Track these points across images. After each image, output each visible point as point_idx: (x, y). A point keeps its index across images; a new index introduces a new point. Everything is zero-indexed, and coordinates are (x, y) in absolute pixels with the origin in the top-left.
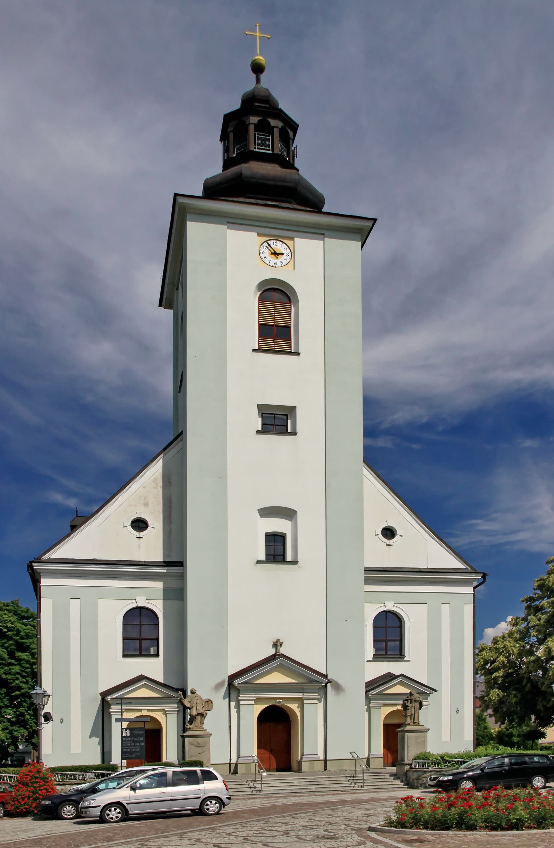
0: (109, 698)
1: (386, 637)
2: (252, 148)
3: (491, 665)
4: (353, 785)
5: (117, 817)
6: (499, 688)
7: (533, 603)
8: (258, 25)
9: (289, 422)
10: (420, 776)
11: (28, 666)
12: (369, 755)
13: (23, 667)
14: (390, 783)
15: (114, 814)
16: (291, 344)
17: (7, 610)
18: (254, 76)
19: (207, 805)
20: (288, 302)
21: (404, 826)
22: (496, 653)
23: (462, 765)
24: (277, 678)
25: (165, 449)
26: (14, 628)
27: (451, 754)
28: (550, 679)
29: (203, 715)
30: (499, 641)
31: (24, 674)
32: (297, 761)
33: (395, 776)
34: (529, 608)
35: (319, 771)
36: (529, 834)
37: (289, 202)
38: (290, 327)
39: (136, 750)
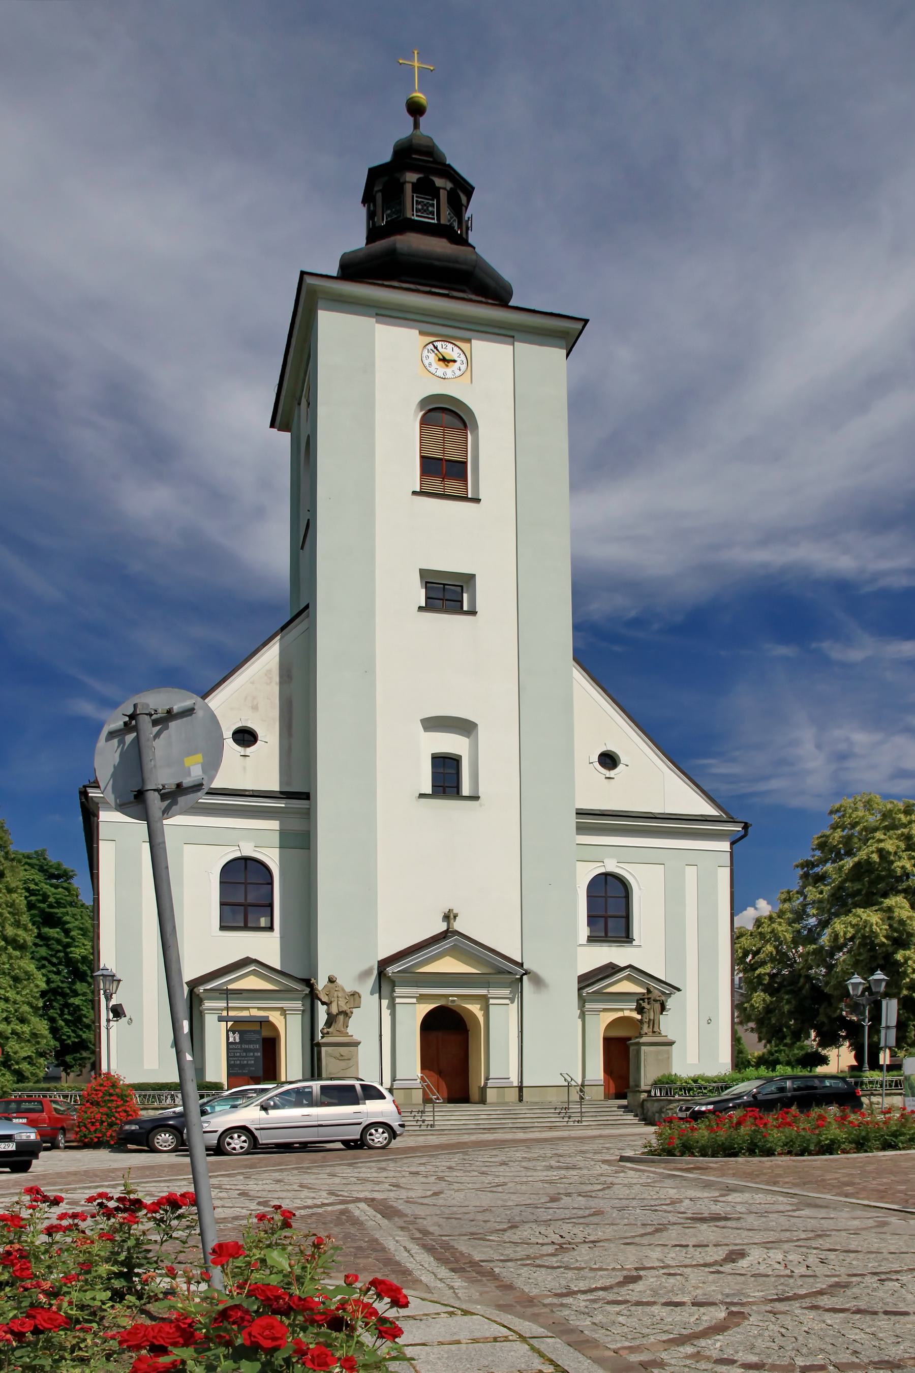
0: (201, 989)
1: (606, 912)
2: (409, 215)
3: (753, 958)
4: (566, 1119)
5: (242, 1148)
6: (764, 991)
7: (812, 869)
8: (416, 52)
9: (465, 596)
10: (663, 1107)
11: (60, 948)
12: (583, 1081)
13: (52, 949)
14: (619, 1118)
15: (238, 1142)
16: (467, 487)
17: (29, 864)
18: (411, 119)
19: (371, 1134)
20: (462, 427)
21: (670, 1153)
22: (760, 940)
23: (723, 1091)
24: (449, 965)
25: (283, 629)
26: (39, 891)
27: (707, 1077)
28: (837, 977)
29: (346, 1015)
30: (763, 923)
31: (55, 960)
32: (479, 1087)
33: (627, 1109)
34: (806, 876)
35: (512, 1102)
36: (848, 1159)
37: (463, 291)
38: (465, 463)
39: (249, 1062)
